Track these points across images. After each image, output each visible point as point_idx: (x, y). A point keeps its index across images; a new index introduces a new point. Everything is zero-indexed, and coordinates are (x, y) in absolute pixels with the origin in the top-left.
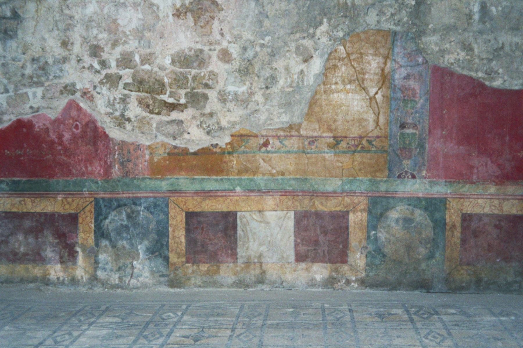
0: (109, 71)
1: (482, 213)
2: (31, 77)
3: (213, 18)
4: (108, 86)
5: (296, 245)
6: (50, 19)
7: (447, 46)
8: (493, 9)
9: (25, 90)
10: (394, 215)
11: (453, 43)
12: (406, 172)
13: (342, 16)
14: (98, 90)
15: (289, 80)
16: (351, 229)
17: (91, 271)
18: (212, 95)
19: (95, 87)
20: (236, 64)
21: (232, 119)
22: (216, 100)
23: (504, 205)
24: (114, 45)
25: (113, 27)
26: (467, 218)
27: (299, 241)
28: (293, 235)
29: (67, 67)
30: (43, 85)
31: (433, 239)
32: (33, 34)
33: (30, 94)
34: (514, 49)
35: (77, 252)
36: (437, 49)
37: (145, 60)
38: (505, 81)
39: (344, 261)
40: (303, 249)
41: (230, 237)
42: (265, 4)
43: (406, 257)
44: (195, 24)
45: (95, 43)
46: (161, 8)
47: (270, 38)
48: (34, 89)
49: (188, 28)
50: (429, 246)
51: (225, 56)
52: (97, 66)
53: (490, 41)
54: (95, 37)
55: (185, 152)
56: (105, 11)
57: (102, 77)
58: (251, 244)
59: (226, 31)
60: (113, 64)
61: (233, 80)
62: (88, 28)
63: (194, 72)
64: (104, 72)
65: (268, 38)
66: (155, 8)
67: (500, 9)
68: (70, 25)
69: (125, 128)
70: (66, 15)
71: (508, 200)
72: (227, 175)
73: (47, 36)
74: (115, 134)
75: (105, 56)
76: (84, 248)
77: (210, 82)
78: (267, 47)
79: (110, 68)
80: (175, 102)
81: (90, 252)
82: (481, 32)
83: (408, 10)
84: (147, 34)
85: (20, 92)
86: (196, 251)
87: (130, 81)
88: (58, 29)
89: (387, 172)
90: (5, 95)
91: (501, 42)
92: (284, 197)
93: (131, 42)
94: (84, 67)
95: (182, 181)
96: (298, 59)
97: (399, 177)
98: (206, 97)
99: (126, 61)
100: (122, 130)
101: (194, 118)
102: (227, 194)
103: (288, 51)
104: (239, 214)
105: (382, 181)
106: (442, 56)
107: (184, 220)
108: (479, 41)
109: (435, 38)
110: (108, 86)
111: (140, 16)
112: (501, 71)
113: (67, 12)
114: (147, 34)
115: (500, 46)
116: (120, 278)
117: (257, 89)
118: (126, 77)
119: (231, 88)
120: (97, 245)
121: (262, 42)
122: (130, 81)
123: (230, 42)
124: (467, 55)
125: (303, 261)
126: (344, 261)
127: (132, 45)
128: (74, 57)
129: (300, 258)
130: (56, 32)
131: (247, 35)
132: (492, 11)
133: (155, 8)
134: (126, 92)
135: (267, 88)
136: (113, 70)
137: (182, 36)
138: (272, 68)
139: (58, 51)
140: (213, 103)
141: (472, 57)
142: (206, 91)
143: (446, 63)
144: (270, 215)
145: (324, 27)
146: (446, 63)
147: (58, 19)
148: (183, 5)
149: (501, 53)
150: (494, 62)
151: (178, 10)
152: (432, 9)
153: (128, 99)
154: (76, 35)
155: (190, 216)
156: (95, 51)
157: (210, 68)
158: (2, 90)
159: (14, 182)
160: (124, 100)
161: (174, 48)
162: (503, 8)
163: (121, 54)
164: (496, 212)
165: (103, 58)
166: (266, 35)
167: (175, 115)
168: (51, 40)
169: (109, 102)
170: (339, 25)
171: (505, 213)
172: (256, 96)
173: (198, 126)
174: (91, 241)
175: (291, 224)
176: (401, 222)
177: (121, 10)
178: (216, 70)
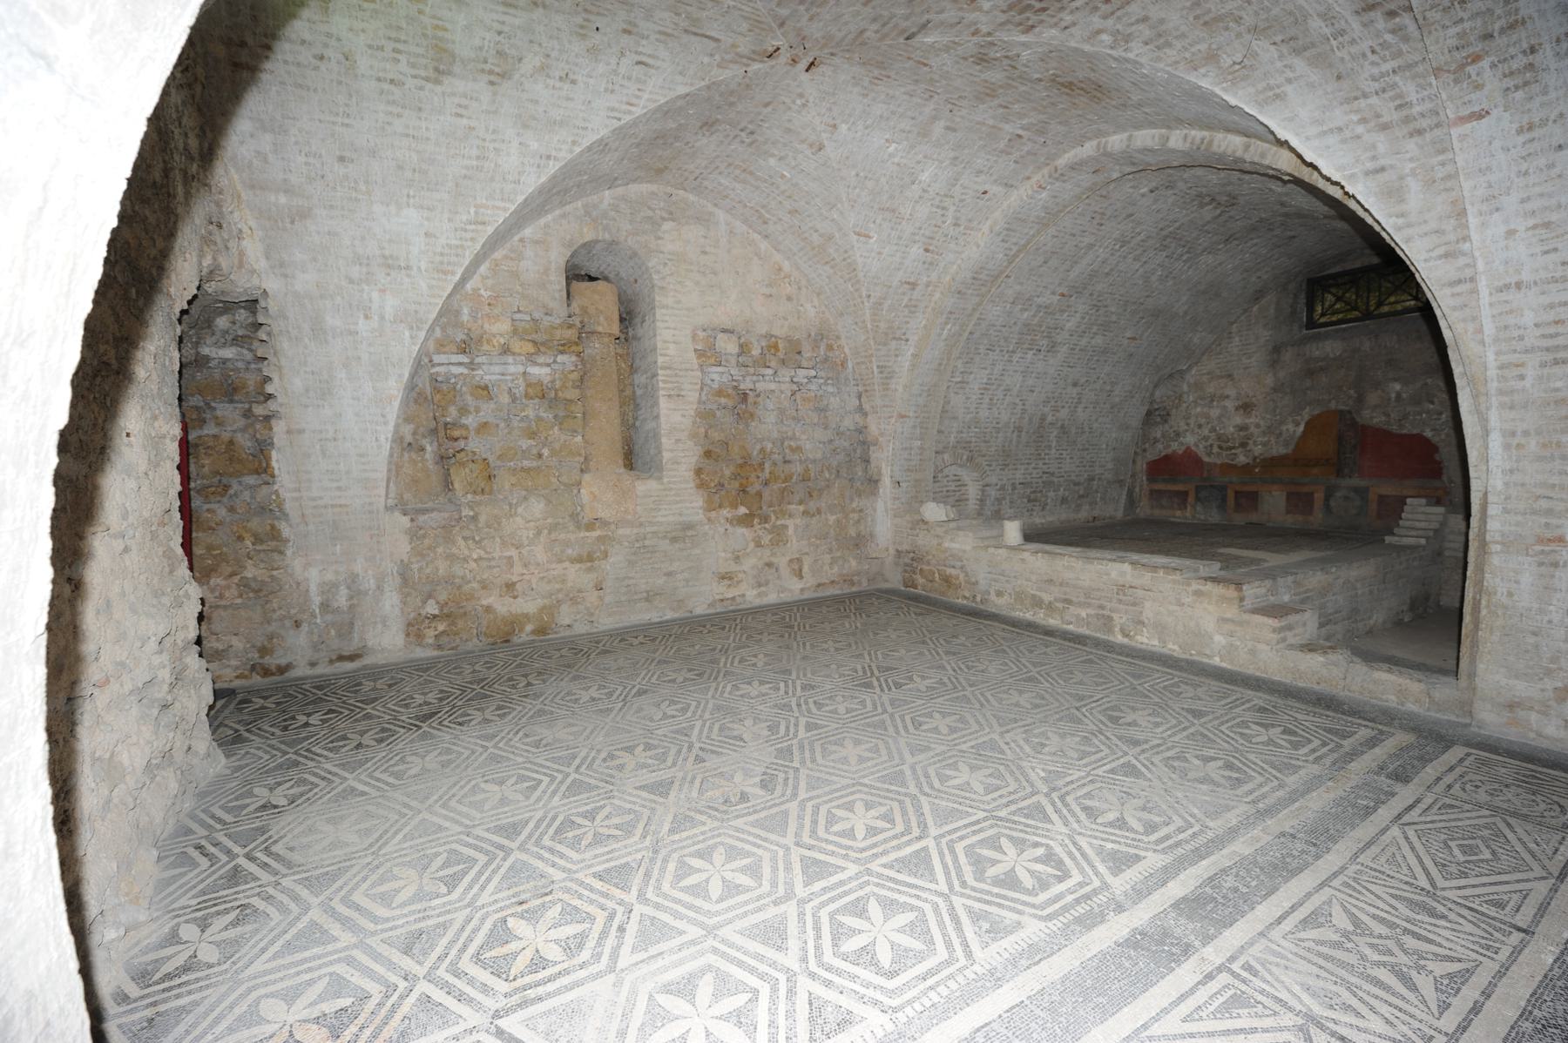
10: (1338, 494)
25: (1207, 416)
55: (1235, 466)
74: (1206, 459)
86: (1238, 507)
129: (1288, 512)
154: (1192, 421)
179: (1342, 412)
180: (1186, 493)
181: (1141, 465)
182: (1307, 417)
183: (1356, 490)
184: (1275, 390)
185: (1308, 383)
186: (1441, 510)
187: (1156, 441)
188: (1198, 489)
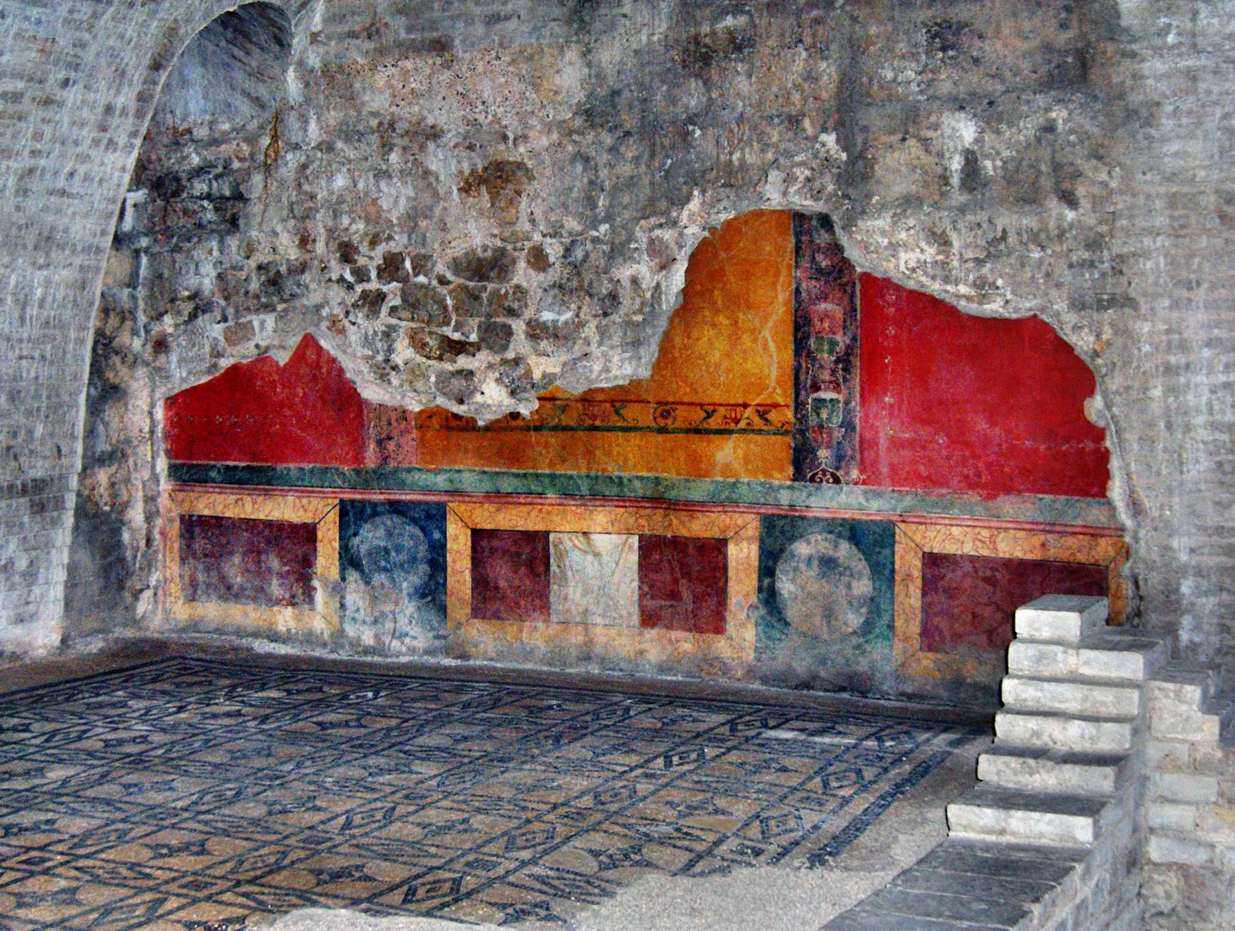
0: (367, 286)
1: (959, 552)
2: (257, 297)
3: (519, 193)
4: (366, 309)
5: (642, 596)
6: (284, 199)
7: (903, 235)
8: (988, 164)
9: (249, 318)
10: (802, 549)
11: (912, 232)
12: (824, 472)
13: (723, 186)
14: (351, 317)
15: (638, 301)
16: (731, 573)
17: (336, 620)
18: (519, 326)
19: (347, 313)
20: (553, 275)
21: (550, 370)
22: (523, 336)
23: (999, 540)
24: (373, 243)
26: (933, 561)
27: (646, 589)
28: (636, 577)
29: (306, 278)
30: (274, 310)
31: (872, 599)
32: (260, 224)
33: (256, 324)
34: (1025, 239)
35: (315, 589)
36: (886, 241)
37: (418, 268)
38: (1007, 302)
39: (719, 630)
40: (651, 604)
41: (537, 575)
42: (450, 221)
43: (825, 629)
44: (492, 205)
45: (346, 239)
46: (442, 178)
47: (607, 226)
48: (262, 316)
49: (481, 213)
50: (864, 610)
51: (538, 259)
52: (349, 277)
53: (979, 225)
54: (346, 229)
55: (466, 425)
56: (361, 185)
57: (356, 296)
58: (571, 590)
59: (538, 214)
60: (373, 275)
61: (550, 300)
62: (336, 215)
63: (491, 286)
64: (359, 289)
65: (604, 228)
66: (432, 179)
67: (999, 163)
68: (311, 209)
69: (390, 383)
70: (306, 193)
71: (1006, 529)
72: (533, 467)
73: (279, 229)
74: (371, 392)
75: (361, 261)
76: (325, 583)
77: (516, 305)
78: (603, 242)
79: (369, 280)
80: (463, 338)
81: (333, 589)
82: (962, 210)
83: (834, 170)
84: (423, 223)
85: (242, 320)
86: (488, 599)
87: (397, 302)
88: (294, 217)
89: (791, 471)
90: (222, 325)
91: (999, 228)
92: (622, 510)
93: (397, 237)
94: (330, 280)
95: (466, 475)
96: (652, 264)
97: (812, 480)
98: (509, 332)
99: (391, 267)
100: (385, 385)
101: (490, 366)
102: (536, 501)
103: (636, 249)
104: (552, 536)
105: (781, 487)
106: (893, 256)
107: (469, 543)
108: (960, 225)
109: (883, 222)
110: (366, 309)
111: (412, 193)
112: (1000, 282)
113: (306, 187)
114: (423, 223)
115: (999, 234)
116: (377, 636)
117: (589, 317)
118: (390, 296)
119: (547, 316)
120: (343, 579)
121: (596, 234)
122: (397, 302)
123: (544, 236)
124: (939, 253)
125: (653, 626)
126: (719, 630)
127: (399, 243)
128: (316, 262)
129: (649, 619)
130: (292, 222)
131: (572, 224)
132: (985, 167)
133: (432, 179)
134: (394, 321)
135: (605, 314)
136: (374, 285)
137: (472, 227)
138: (611, 280)
139: (294, 254)
140: (520, 344)
141: (947, 257)
142: (509, 321)
143: (902, 268)
144: (603, 542)
145: (694, 205)
146: (902, 268)
147: (294, 199)
148: (473, 172)
149: (1002, 247)
150: (988, 265)
151: (467, 182)
152: (876, 167)
153: (394, 334)
154: (319, 227)
155: (478, 535)
156: (347, 253)
157: (515, 281)
158: (219, 318)
159: (227, 468)
160: (388, 334)
161: (458, 249)
162: (1005, 163)
163: (385, 258)
164: (985, 552)
165: (359, 264)
166: (601, 222)
167: (463, 362)
168: (286, 234)
169: (366, 337)
170: (719, 201)
171: (1001, 555)
172: (586, 330)
173: (497, 380)
174: (334, 573)
175: (634, 558)
176: (815, 563)
177: (383, 185)
178: (525, 284)
179: (799, 218)
180: (307, 534)
181: (144, 410)
182: (694, 233)
183: (854, 532)
184: (591, 115)
185: (693, 97)
186: (1131, 665)
187: (200, 306)
188: (352, 516)
